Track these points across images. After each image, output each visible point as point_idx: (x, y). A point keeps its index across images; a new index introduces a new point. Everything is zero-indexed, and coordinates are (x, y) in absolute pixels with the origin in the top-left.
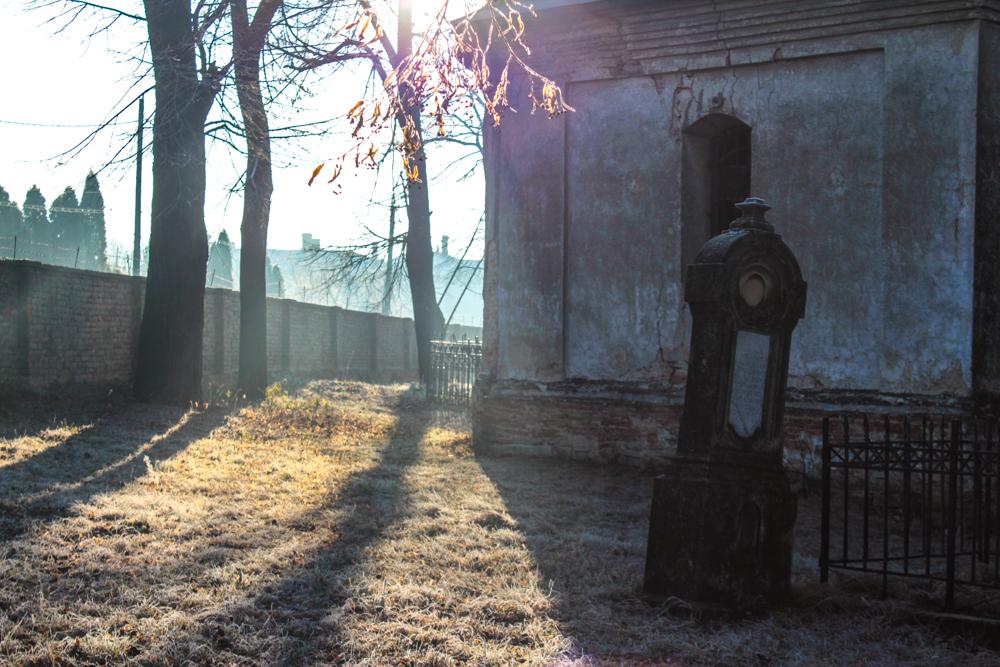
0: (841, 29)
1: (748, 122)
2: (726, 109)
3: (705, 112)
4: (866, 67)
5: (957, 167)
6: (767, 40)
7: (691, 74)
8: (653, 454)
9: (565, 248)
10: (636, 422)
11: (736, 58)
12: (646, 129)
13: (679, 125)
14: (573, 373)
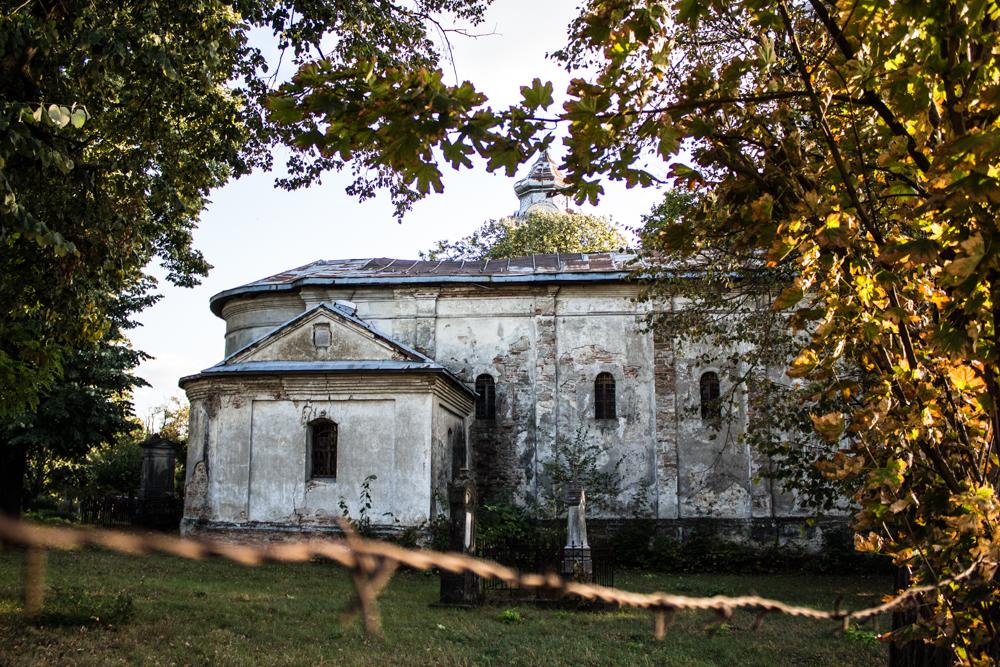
2: (327, 417)
3: (317, 416)
4: (387, 405)
7: (311, 401)
11: (332, 397)
13: (305, 421)
14: (252, 519)
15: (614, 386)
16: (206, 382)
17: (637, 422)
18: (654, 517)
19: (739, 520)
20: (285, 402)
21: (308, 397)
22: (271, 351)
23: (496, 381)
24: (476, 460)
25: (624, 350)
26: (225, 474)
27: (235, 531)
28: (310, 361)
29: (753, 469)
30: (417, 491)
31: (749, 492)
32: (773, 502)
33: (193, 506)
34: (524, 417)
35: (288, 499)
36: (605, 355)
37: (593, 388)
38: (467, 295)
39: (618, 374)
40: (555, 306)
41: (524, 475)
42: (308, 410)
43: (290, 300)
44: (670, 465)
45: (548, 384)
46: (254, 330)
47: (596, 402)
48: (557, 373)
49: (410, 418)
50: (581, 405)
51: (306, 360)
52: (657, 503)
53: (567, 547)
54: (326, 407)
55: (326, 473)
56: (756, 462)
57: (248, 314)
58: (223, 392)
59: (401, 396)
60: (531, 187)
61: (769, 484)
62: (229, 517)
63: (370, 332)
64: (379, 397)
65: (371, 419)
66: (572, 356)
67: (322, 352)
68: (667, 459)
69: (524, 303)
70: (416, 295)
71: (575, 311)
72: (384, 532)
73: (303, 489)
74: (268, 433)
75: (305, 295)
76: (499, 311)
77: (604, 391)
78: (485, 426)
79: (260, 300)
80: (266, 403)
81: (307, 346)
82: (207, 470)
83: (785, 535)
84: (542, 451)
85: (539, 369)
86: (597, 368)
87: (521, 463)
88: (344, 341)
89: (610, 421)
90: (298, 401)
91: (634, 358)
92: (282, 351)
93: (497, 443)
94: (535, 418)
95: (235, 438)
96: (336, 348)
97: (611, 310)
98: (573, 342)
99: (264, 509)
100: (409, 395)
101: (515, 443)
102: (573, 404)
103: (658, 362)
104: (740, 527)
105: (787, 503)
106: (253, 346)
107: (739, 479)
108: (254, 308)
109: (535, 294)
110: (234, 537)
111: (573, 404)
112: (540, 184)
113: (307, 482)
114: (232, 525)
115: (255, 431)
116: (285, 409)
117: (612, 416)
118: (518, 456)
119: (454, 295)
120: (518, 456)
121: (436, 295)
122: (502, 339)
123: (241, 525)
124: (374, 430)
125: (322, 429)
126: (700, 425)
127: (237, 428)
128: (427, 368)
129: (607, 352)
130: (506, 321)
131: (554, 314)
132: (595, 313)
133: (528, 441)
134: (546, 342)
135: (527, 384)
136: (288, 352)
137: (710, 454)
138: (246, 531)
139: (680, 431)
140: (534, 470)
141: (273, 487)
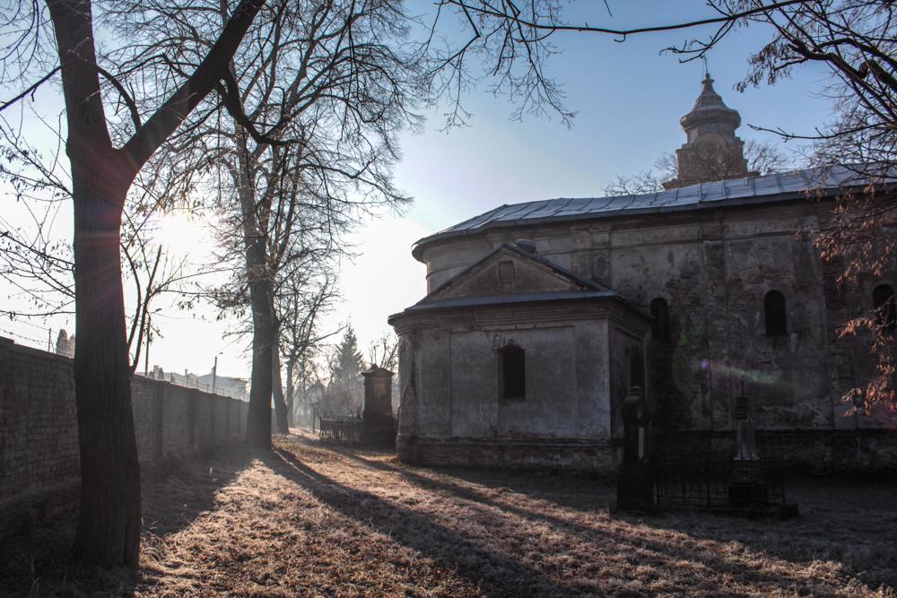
1: (523, 348)
2: (515, 344)
7: (501, 331)
10: (484, 452)
11: (519, 326)
13: (496, 348)
14: (453, 435)
17: (808, 337)
21: (498, 327)
23: (669, 303)
25: (792, 268)
34: (697, 337)
38: (637, 226)
41: (700, 390)
42: (498, 338)
54: (514, 336)
64: (559, 324)
66: (741, 277)
69: (692, 230)
70: (591, 230)
77: (774, 306)
86: (766, 287)
90: (489, 331)
102: (744, 322)
109: (701, 221)
111: (744, 322)
119: (626, 227)
121: (609, 228)
123: (446, 440)
129: (774, 272)
140: (708, 385)
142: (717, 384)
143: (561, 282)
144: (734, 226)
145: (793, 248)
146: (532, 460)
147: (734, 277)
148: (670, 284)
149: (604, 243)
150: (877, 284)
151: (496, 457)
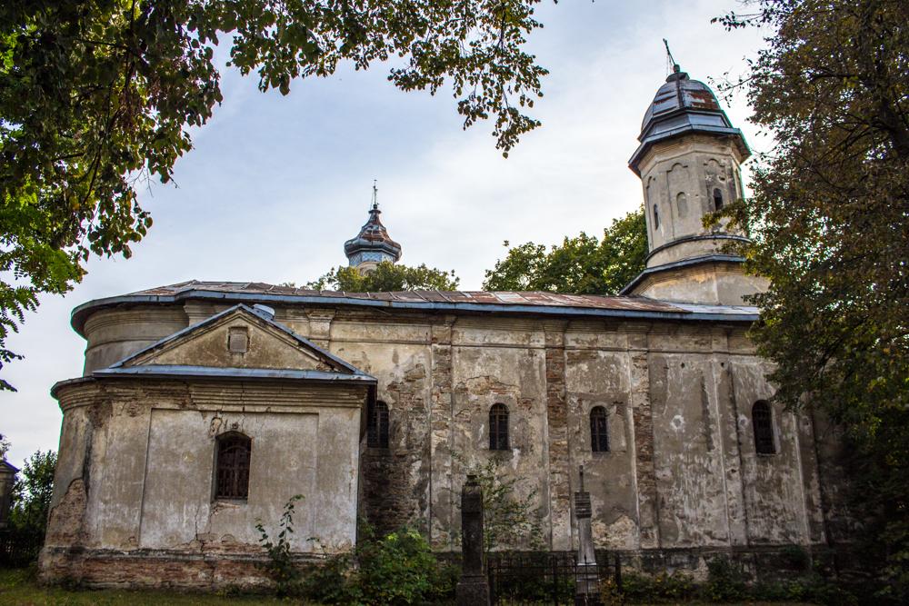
0: (300, 404)
1: (250, 436)
2: (240, 430)
3: (228, 430)
4: (309, 421)
5: (350, 463)
6: (265, 403)
7: (222, 412)
8: (194, 584)
9: (144, 485)
10: (185, 569)
11: (247, 409)
12: (195, 434)
13: (214, 434)
14: (143, 545)
15: (506, 418)
16: (93, 386)
17: (530, 453)
18: (548, 550)
19: (629, 552)
20: (191, 412)
21: (219, 407)
22: (177, 354)
23: (390, 407)
24: (368, 490)
25: (517, 383)
26: (113, 493)
27: (121, 559)
28: (222, 367)
29: (640, 501)
30: (342, 514)
31: (637, 524)
32: (660, 532)
33: (64, 531)
34: (418, 446)
35: (189, 522)
36: (500, 386)
37: (488, 418)
38: (363, 319)
39: (512, 406)
40: (452, 335)
41: (417, 506)
42: (217, 421)
43: (169, 314)
44: (562, 497)
45: (442, 413)
46: (125, 344)
47: (490, 434)
48: (453, 403)
49: (335, 434)
50: (476, 435)
51: (218, 367)
52: (551, 535)
53: (579, 564)
54: (239, 420)
55: (232, 495)
56: (644, 494)
57: (120, 327)
58: (118, 398)
59: (325, 410)
60: (362, 246)
61: (656, 515)
62: (115, 544)
63: (294, 338)
64: (300, 410)
65: (290, 434)
66: (467, 386)
67: (237, 358)
68: (560, 491)
69: (422, 332)
70: (310, 316)
71: (470, 341)
72: (303, 560)
73: (208, 512)
74: (168, 445)
75: (188, 309)
76: (395, 337)
77: (499, 416)
78: (377, 454)
79: (137, 312)
80: (167, 413)
81: (220, 351)
82: (87, 488)
83: (671, 566)
84: (436, 481)
85: (435, 398)
86: (491, 398)
87: (415, 493)
88: (263, 348)
89: (506, 452)
90: (206, 411)
91: (527, 390)
92: (190, 354)
93: (390, 472)
94: (430, 447)
95: (128, 451)
96: (254, 354)
97: (506, 343)
98: (468, 372)
99: (159, 534)
100: (334, 409)
101: (408, 473)
102: (468, 434)
103: (550, 394)
104: (630, 558)
105: (672, 534)
106: (158, 347)
107: (628, 511)
108: (128, 321)
109: (431, 323)
110: (120, 567)
111: (468, 434)
112: (370, 244)
113: (212, 503)
114: (118, 553)
115: (153, 444)
116: (190, 419)
117: (506, 447)
118: (412, 486)
119: (349, 319)
120: (412, 486)
121: (331, 317)
122: (397, 366)
123: (130, 553)
124: (294, 446)
125: (230, 444)
126: (590, 457)
127: (131, 439)
128: (359, 380)
129: (501, 384)
130: (401, 348)
131: (450, 343)
132: (490, 345)
133: (422, 471)
134: (442, 371)
135: (422, 412)
136: (197, 356)
137: (600, 485)
138: (136, 560)
139: (571, 463)
140: (428, 500)
141: (172, 508)
142: (437, 500)
143: (308, 360)
144: (463, 333)
145: (519, 361)
146: (252, 580)
147: (460, 386)
148: (393, 387)
149: (323, 334)
150: (594, 405)
151: (202, 575)
